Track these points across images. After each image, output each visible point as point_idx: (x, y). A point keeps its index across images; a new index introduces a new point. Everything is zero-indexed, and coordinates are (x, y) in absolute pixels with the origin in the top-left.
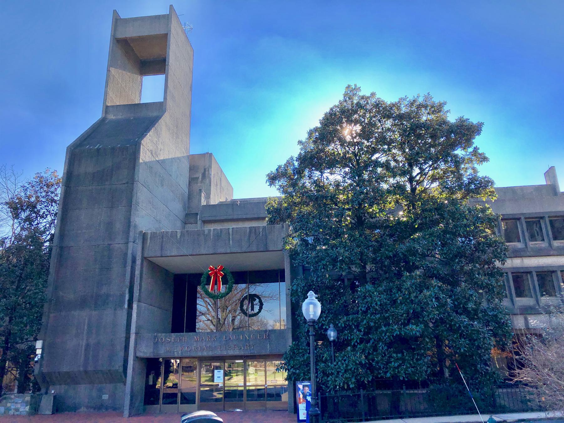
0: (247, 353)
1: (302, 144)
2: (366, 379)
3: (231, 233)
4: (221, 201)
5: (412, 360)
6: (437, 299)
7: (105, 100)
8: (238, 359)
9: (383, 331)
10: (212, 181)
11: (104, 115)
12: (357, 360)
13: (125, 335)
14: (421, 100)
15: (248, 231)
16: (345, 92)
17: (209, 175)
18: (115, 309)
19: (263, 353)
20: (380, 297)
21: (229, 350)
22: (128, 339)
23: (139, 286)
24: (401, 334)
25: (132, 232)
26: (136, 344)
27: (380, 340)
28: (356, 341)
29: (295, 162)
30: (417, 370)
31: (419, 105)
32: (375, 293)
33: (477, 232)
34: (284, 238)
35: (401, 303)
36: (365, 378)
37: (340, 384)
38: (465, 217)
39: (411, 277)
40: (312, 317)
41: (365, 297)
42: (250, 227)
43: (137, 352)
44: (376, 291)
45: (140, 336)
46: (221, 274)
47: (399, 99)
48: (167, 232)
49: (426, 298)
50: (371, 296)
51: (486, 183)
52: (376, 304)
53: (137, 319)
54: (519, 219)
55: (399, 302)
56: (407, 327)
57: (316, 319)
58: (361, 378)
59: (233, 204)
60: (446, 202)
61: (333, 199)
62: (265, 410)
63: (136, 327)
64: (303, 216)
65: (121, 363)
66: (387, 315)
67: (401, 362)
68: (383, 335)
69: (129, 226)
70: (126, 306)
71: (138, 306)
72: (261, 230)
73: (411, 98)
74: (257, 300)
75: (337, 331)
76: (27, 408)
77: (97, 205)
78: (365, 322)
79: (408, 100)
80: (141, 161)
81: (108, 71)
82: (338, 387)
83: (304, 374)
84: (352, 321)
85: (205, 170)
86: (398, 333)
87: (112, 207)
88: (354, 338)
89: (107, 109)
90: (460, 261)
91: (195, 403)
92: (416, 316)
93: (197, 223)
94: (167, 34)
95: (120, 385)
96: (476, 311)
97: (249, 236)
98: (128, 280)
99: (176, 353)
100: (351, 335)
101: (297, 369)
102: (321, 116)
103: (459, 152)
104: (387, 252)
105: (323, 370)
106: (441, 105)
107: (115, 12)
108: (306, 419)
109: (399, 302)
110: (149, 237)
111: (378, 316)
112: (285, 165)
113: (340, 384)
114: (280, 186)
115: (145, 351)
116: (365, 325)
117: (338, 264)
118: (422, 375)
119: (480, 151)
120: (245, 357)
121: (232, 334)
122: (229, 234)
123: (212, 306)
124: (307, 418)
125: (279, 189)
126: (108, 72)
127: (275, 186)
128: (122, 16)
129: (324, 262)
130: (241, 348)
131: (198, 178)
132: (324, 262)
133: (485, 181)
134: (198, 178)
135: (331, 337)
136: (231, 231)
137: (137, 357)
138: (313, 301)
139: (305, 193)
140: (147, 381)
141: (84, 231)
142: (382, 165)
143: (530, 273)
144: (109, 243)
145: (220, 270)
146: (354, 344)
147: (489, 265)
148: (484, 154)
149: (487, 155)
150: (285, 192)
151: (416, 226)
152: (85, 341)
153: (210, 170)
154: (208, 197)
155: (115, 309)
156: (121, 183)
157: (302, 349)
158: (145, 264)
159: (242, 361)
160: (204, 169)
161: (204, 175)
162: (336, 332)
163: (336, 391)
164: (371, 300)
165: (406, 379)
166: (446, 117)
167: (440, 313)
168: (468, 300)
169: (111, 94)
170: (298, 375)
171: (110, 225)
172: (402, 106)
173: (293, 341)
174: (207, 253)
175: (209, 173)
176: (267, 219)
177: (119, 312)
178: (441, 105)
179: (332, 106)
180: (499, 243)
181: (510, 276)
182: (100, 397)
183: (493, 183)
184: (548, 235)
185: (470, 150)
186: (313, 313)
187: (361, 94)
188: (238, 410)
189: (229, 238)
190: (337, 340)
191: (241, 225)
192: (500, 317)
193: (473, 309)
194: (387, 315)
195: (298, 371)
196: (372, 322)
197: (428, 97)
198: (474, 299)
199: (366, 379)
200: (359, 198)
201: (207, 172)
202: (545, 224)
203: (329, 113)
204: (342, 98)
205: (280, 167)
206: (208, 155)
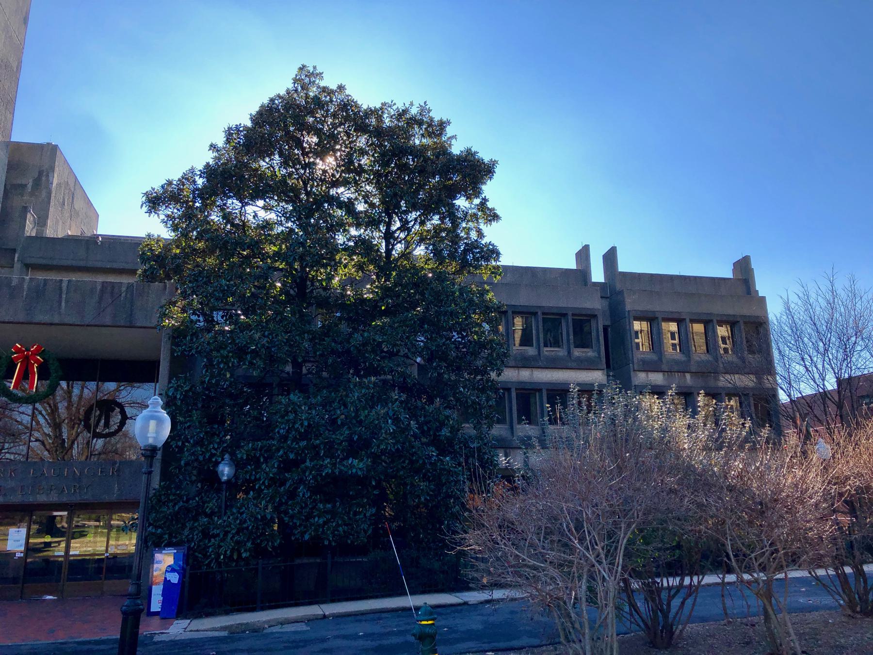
0: (76, 499)
1: (218, 151)
2: (270, 544)
4: (70, 234)
5: (349, 513)
6: (396, 420)
9: (307, 467)
10: (53, 195)
12: (258, 513)
14: (414, 111)
16: (296, 76)
17: (49, 183)
19: (106, 498)
20: (310, 414)
21: (38, 493)
24: (333, 472)
27: (301, 481)
28: (264, 483)
29: (197, 178)
30: (352, 529)
31: (411, 119)
32: (303, 408)
33: (467, 325)
34: (161, 307)
35: (343, 424)
36: (268, 542)
37: (226, 551)
38: (454, 301)
39: (361, 385)
40: (151, 441)
41: (287, 413)
42: (103, 282)
44: (305, 404)
46: (37, 361)
47: (382, 104)
49: (378, 419)
50: (295, 412)
51: (493, 252)
52: (302, 425)
54: (535, 314)
55: (339, 422)
56: (345, 463)
57: (160, 445)
58: (261, 541)
59: (91, 243)
60: (430, 275)
61: (255, 246)
64: (200, 272)
66: (318, 442)
67: (329, 516)
68: (307, 474)
72: (124, 289)
73: (400, 106)
75: (236, 466)
78: (281, 453)
79: (395, 107)
82: (222, 557)
83: (170, 535)
84: (261, 450)
85: (40, 173)
86: (330, 471)
88: (260, 477)
90: (439, 366)
92: (355, 449)
93: (13, 267)
96: (450, 441)
97: (101, 298)
100: (257, 473)
101: (159, 527)
102: (255, 109)
103: (461, 202)
104: (333, 344)
105: (203, 529)
106: (442, 125)
108: (160, 610)
109: (339, 422)
111: (303, 444)
112: (179, 180)
113: (226, 551)
114: (168, 216)
116: (282, 456)
117: (249, 357)
118: (358, 537)
119: (490, 205)
120: (71, 506)
122: (61, 289)
123: (47, 417)
124: (162, 609)
125: (163, 221)
127: (158, 215)
129: (224, 352)
130: (63, 491)
131: (24, 186)
132: (224, 352)
133: (488, 250)
134: (24, 186)
135: (223, 475)
136: (64, 285)
138: (156, 414)
139: (208, 232)
142: (341, 205)
143: (540, 390)
145: (35, 353)
146: (260, 487)
147: (483, 375)
148: (494, 209)
149: (498, 212)
150: (175, 228)
151: (383, 308)
154: (42, 221)
157: (174, 495)
159: (65, 513)
160: (39, 172)
162: (234, 467)
163: (219, 564)
164: (295, 417)
165: (334, 544)
166: (450, 145)
167: (398, 442)
168: (442, 425)
170: (160, 537)
172: (385, 116)
173: (161, 481)
174: (12, 319)
175: (48, 180)
176: (139, 272)
178: (442, 125)
179: (272, 96)
180: (497, 344)
181: (514, 394)
183: (498, 254)
184: (568, 340)
185: (477, 201)
186: (154, 435)
187: (323, 84)
189: (61, 297)
190: (233, 480)
191: (87, 278)
192: (484, 451)
193: (447, 438)
194: (318, 442)
195: (159, 531)
196: (292, 452)
197: (423, 109)
198: (451, 423)
199: (270, 544)
200: (296, 253)
201: (44, 178)
202: (567, 322)
203: (268, 106)
204: (290, 86)
205: (170, 183)
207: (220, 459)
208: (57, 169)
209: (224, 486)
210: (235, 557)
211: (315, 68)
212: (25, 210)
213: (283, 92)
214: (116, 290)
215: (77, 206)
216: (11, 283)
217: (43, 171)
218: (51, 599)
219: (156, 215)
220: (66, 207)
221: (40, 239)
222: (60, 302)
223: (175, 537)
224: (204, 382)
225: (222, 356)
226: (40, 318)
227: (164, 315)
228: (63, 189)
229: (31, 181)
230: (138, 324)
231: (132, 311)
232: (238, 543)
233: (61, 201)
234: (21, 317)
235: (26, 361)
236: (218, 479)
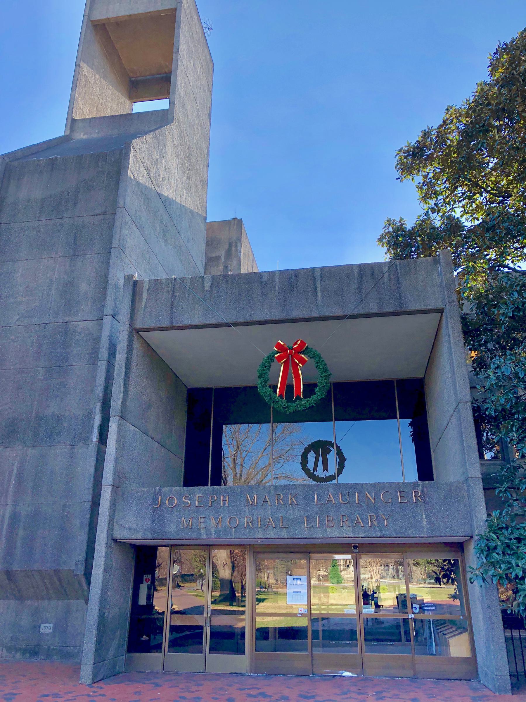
3: (318, 277)
7: (71, 109)
8: (339, 553)
10: (242, 263)
11: (68, 133)
13: (90, 498)
15: (356, 271)
17: (238, 252)
18: (73, 446)
22: (95, 504)
23: (122, 385)
25: (111, 297)
26: (114, 511)
43: (116, 527)
45: (123, 494)
48: (182, 279)
53: (116, 453)
62: (414, 678)
63: (115, 472)
65: (81, 556)
69: (105, 288)
70: (95, 438)
71: (119, 426)
72: (386, 269)
74: (334, 452)
77: (45, 252)
80: (129, 174)
81: (77, 65)
85: (230, 245)
87: (74, 256)
89: (72, 123)
91: (243, 653)
94: (175, 10)
95: (76, 604)
98: (99, 388)
99: (203, 531)
110: (145, 289)
115: (135, 526)
120: (355, 547)
121: (335, 490)
122: (314, 278)
126: (78, 67)
131: (218, 258)
137: (115, 540)
141: (20, 299)
144: (67, 319)
153: (239, 244)
155: (73, 446)
156: (91, 214)
158: (137, 345)
159: (349, 557)
161: (229, 253)
169: (80, 103)
174: (267, 318)
177: (79, 450)
182: (36, 628)
188: (346, 674)
189: (315, 287)
201: (234, 249)
206: (236, 222)
214: (377, 272)
217: (232, 242)
222: (316, 292)
226: (296, 313)
229: (223, 252)
230: (411, 308)
231: (400, 293)
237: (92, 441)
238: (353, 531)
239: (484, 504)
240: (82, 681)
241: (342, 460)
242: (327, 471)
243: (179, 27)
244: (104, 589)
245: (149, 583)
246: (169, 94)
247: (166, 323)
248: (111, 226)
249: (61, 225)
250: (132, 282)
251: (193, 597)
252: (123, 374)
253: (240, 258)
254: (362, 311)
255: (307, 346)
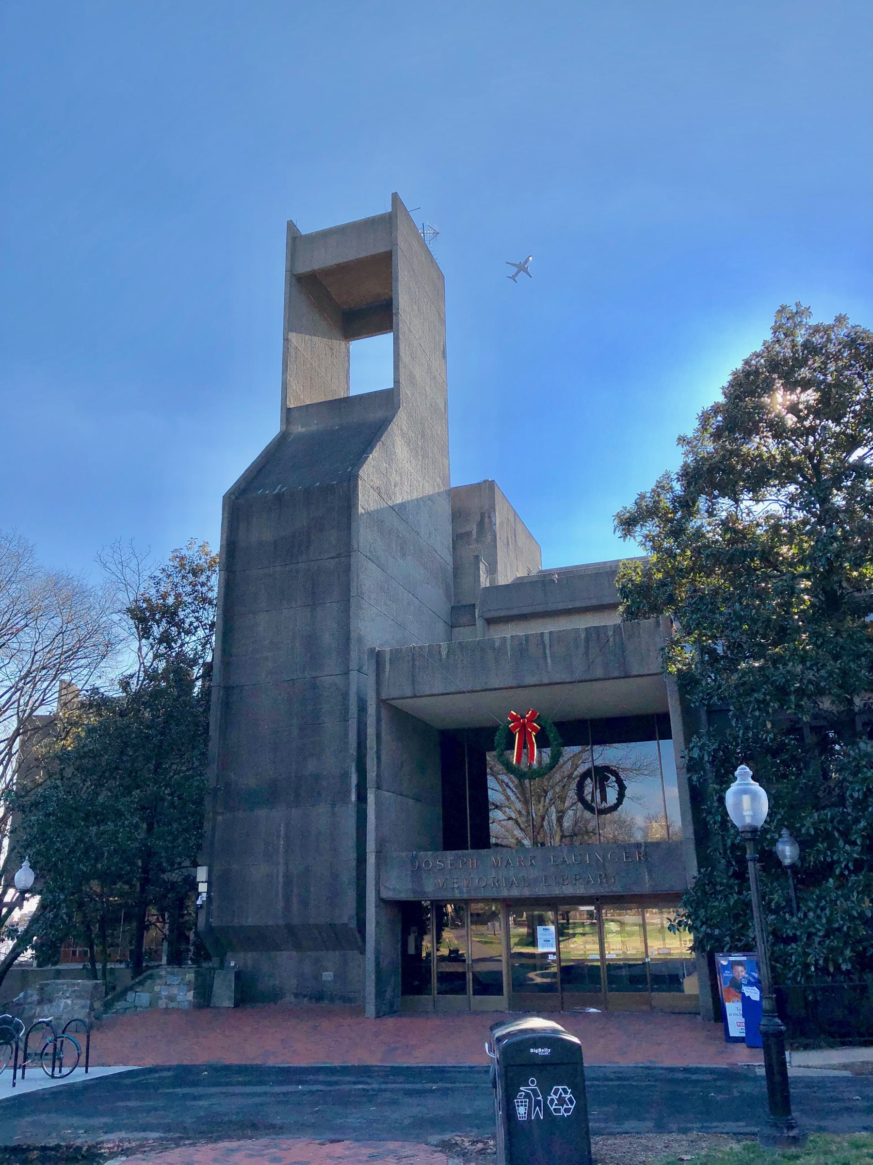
0: (603, 890)
1: (688, 443)
3: (547, 641)
10: (498, 536)
16: (776, 322)
17: (492, 524)
18: (333, 805)
19: (636, 890)
21: (563, 885)
22: (361, 860)
23: (375, 759)
28: (847, 867)
37: (816, 961)
40: (748, 820)
42: (586, 629)
43: (382, 888)
46: (534, 729)
61: (768, 556)
70: (353, 797)
71: (376, 797)
72: (611, 633)
76: (190, 996)
80: (361, 510)
81: (286, 340)
84: (832, 821)
85: (482, 515)
89: (288, 414)
93: (475, 625)
97: (587, 648)
99: (456, 891)
100: (833, 853)
107: (291, 226)
112: (653, 491)
114: (646, 537)
117: (793, 698)
120: (597, 899)
128: (305, 229)
130: (588, 882)
131: (469, 534)
134: (469, 534)
135: (785, 857)
136: (547, 638)
140: (405, 945)
144: (314, 674)
145: (530, 720)
150: (656, 548)
152: (281, 868)
154: (492, 570)
155: (333, 805)
159: (592, 908)
161: (481, 524)
162: (797, 845)
163: (808, 978)
169: (294, 386)
171: (311, 641)
173: (700, 866)
179: (747, 356)
187: (813, 322)
188: (592, 1010)
189: (545, 653)
201: (486, 520)
204: (769, 336)
205: (642, 497)
207: (777, 836)
208: (497, 508)
209: (789, 871)
210: (831, 970)
211: (798, 305)
212: (477, 558)
213: (759, 348)
215: (520, 544)
216: (494, 644)
218: (594, 1013)
219: (632, 538)
220: (511, 547)
221: (495, 589)
223: (740, 940)
224: (738, 736)
225: (758, 701)
226: (530, 680)
227: (670, 659)
228: (505, 526)
229: (475, 526)
231: (624, 658)
232: (832, 950)
233: (506, 541)
234: (510, 682)
235: (524, 734)
236: (779, 863)
237: (351, 800)
238: (585, 888)
239: (695, 862)
240: (367, 1015)
241: (622, 788)
242: (606, 802)
243: (397, 281)
244: (377, 942)
245: (416, 934)
246: (392, 327)
247: (410, 694)
248: (348, 569)
249: (297, 572)
250: (375, 655)
251: (480, 944)
252: (375, 746)
253: (495, 531)
254: (588, 677)
255: (539, 715)
